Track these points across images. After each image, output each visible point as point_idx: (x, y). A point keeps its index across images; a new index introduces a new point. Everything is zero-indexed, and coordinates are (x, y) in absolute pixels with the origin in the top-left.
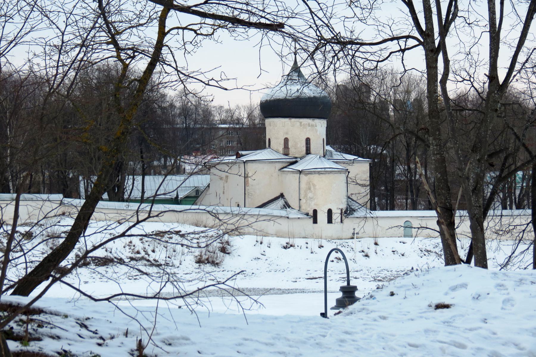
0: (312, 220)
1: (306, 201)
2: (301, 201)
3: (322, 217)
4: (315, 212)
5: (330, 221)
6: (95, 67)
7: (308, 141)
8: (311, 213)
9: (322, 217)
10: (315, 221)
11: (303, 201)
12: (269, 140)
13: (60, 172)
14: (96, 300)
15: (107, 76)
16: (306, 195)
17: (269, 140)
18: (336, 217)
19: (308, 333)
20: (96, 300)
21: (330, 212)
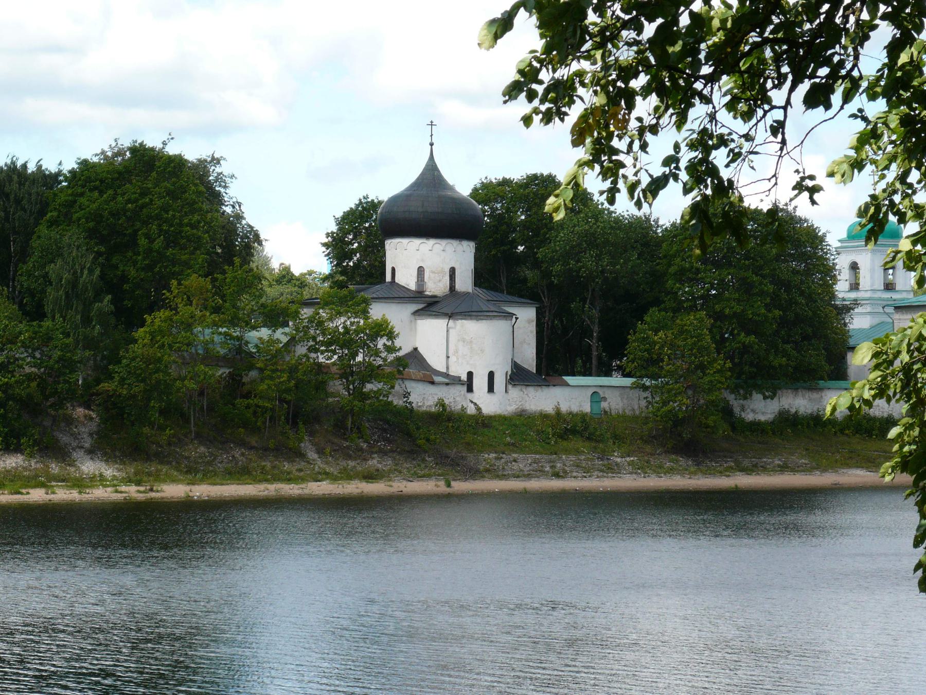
0: (465, 388)
1: (458, 359)
2: (450, 359)
3: (480, 383)
4: (470, 375)
5: (491, 389)
6: (677, 111)
7: (453, 271)
8: (464, 377)
9: (480, 383)
10: (470, 389)
11: (453, 359)
12: (393, 270)
13: (887, 267)
14: (833, 118)
15: (788, 281)
16: (456, 352)
17: (393, 270)
18: (500, 381)
19: (117, 491)
20: (833, 118)
21: (491, 375)
